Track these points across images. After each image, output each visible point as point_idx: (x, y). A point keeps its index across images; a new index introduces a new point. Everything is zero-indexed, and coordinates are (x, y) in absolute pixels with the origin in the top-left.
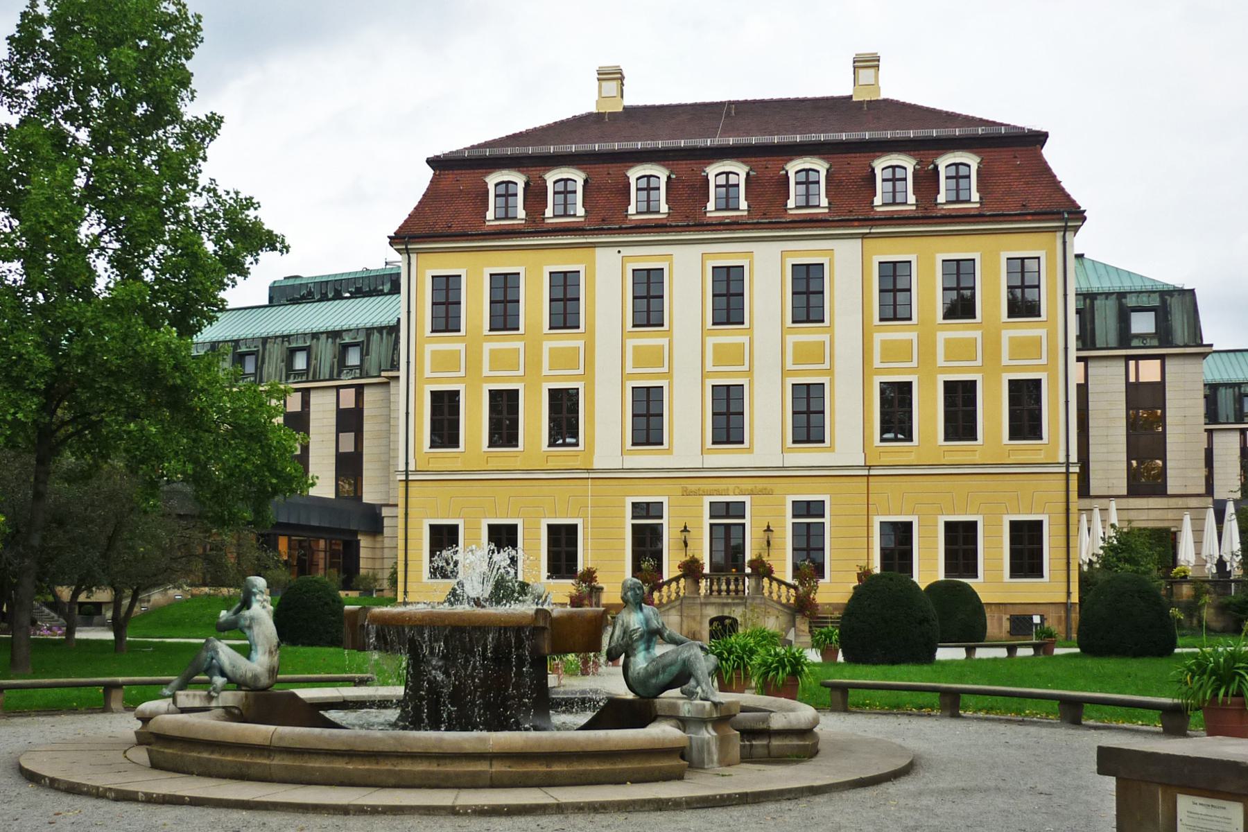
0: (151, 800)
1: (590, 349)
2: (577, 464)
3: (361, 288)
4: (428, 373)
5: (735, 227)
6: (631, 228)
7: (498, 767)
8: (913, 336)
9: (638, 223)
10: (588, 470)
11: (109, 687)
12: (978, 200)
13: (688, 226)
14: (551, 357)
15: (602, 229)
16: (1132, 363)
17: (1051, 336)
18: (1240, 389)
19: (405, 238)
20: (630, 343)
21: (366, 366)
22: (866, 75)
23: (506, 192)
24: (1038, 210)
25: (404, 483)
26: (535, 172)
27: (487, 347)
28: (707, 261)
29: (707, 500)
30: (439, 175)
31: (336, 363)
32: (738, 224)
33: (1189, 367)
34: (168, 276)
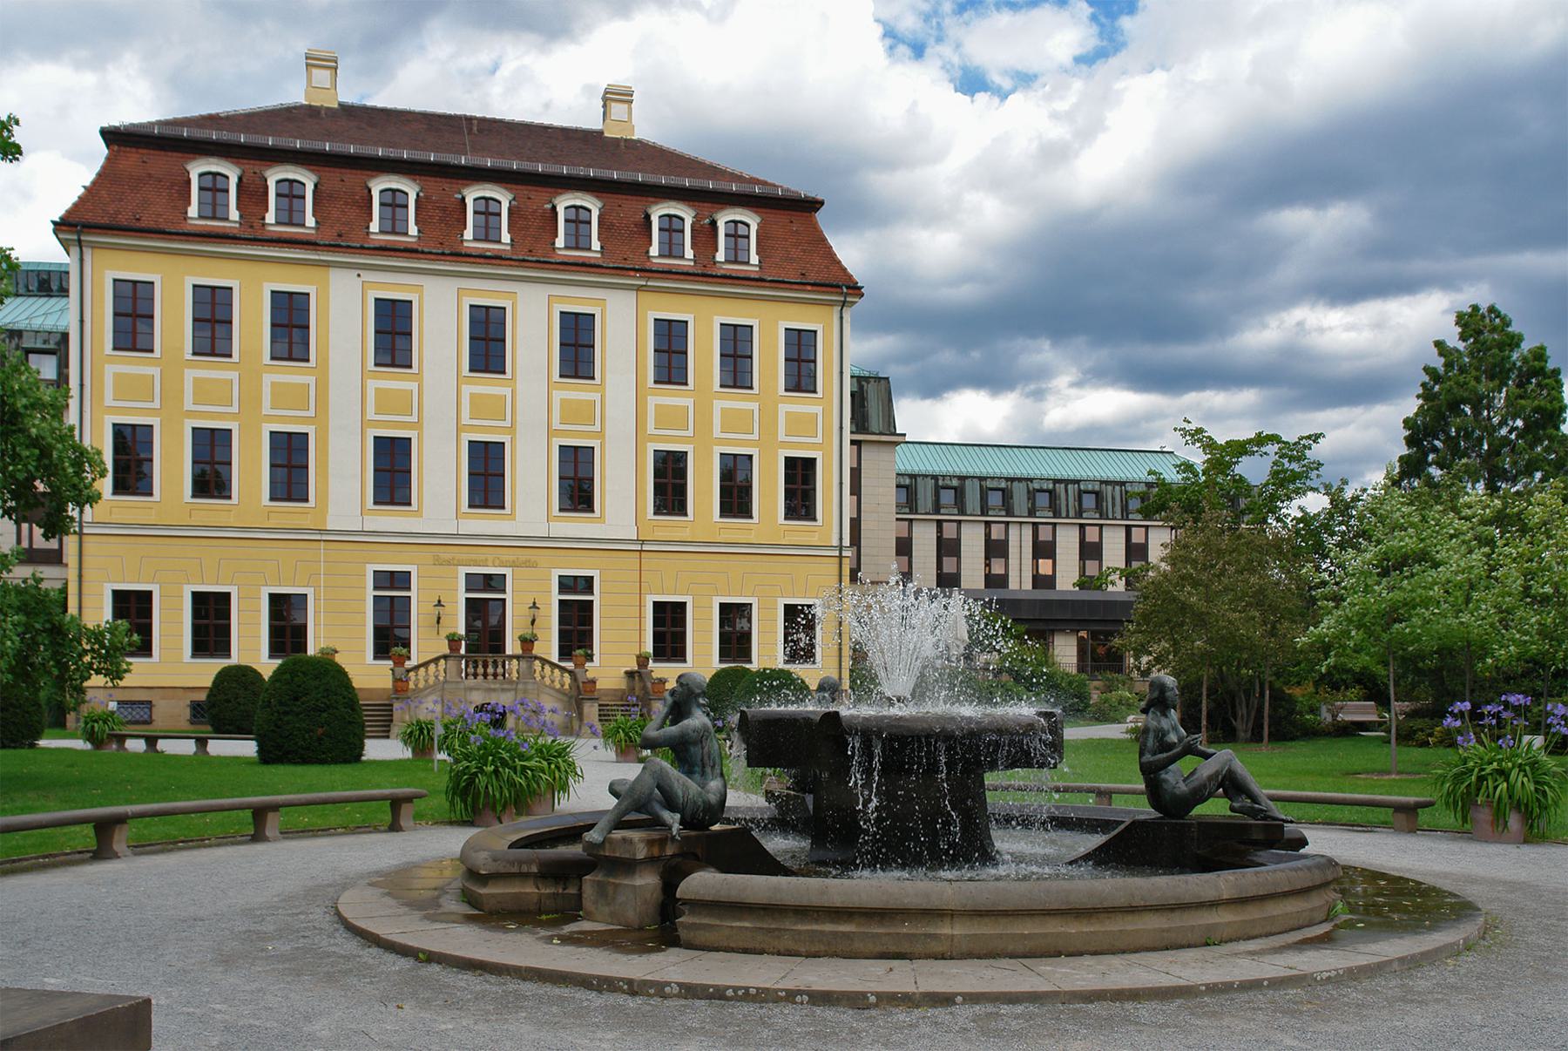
4: (109, 401)
5: (498, 262)
8: (688, 402)
9: (383, 244)
13: (443, 254)
14: (273, 394)
22: (618, 110)
26: (253, 166)
27: (783, 408)
34: (1534, 380)
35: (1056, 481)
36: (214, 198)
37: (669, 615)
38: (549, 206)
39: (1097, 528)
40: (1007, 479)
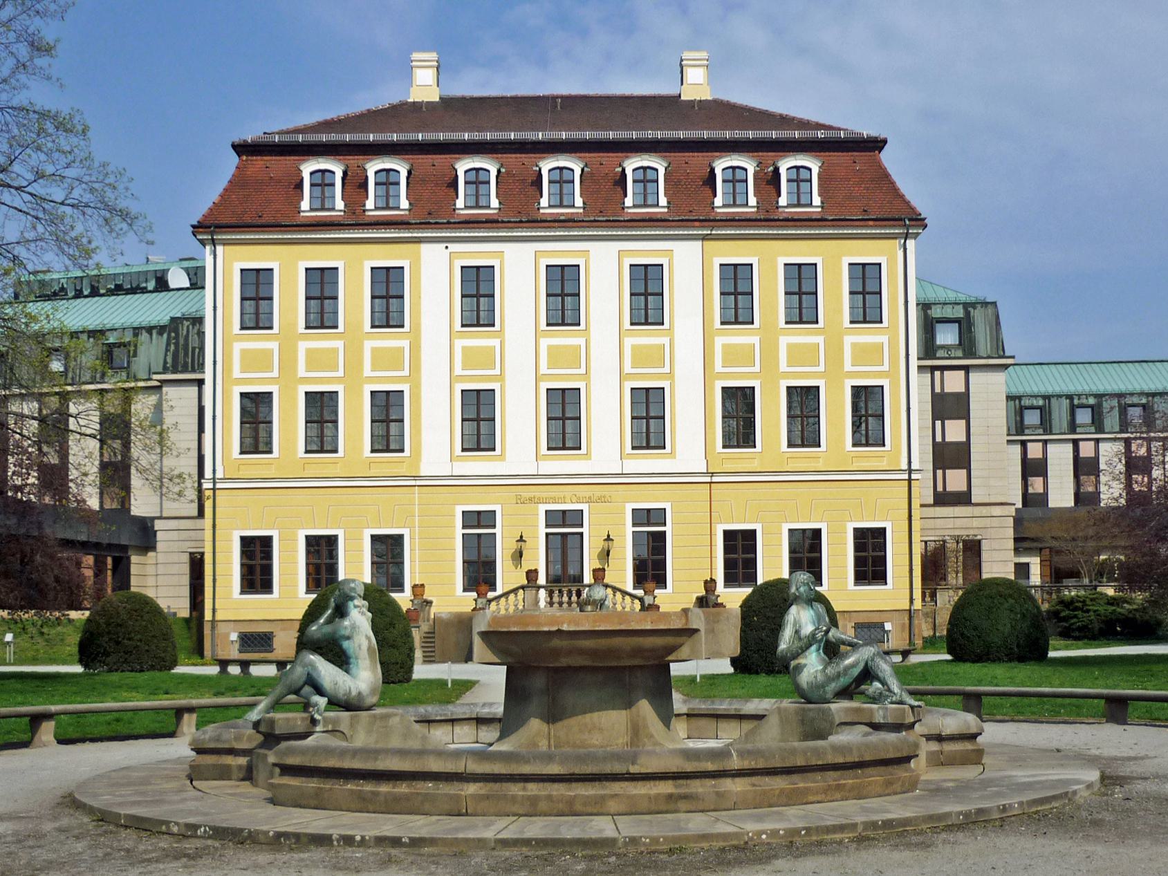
0: (281, 841)
1: (415, 348)
4: (237, 373)
6: (459, 223)
10: (415, 477)
11: (179, 712)
12: (819, 204)
13: (521, 222)
15: (429, 223)
16: (937, 373)
17: (893, 343)
18: (1020, 402)
20: (629, 342)
21: (134, 367)
23: (322, 181)
24: (890, 216)
26: (354, 160)
27: (303, 346)
28: (456, 261)
29: (543, 508)
30: (246, 160)
33: (999, 378)
36: (323, 192)
37: (740, 543)
38: (620, 169)
40: (1148, 395)
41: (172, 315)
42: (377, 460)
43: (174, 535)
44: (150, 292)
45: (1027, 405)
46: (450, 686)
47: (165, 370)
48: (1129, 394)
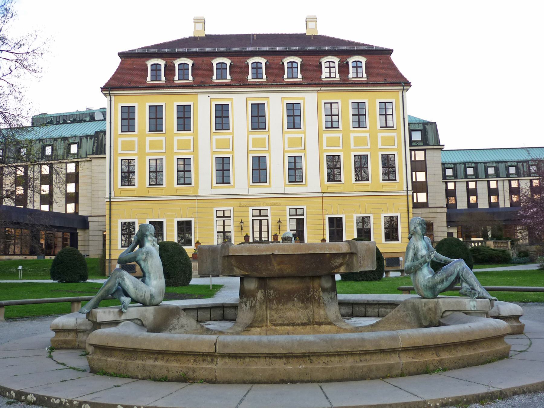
1: (196, 140)
2: (191, 193)
3: (76, 119)
4: (120, 151)
6: (214, 86)
7: (404, 359)
13: (240, 85)
15: (201, 86)
19: (108, 88)
22: (311, 25)
24: (394, 82)
25: (109, 202)
26: (169, 60)
27: (148, 139)
28: (213, 102)
30: (124, 60)
31: (65, 153)
32: (262, 85)
35: (518, 162)
37: (335, 223)
38: (281, 63)
39: (333, 127)
40: (496, 162)
41: (96, 131)
42: (180, 188)
43: (97, 224)
44: (88, 122)
45: (447, 167)
46: (211, 288)
47: (93, 154)
48: (489, 162)
